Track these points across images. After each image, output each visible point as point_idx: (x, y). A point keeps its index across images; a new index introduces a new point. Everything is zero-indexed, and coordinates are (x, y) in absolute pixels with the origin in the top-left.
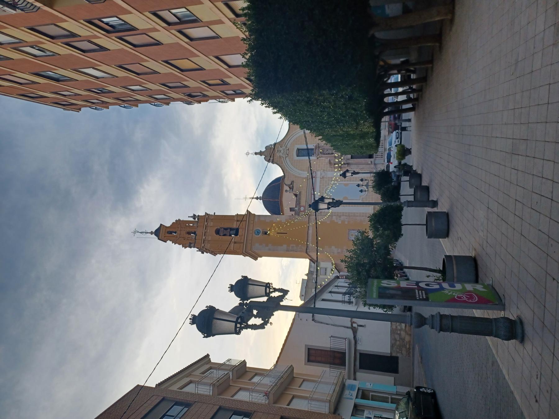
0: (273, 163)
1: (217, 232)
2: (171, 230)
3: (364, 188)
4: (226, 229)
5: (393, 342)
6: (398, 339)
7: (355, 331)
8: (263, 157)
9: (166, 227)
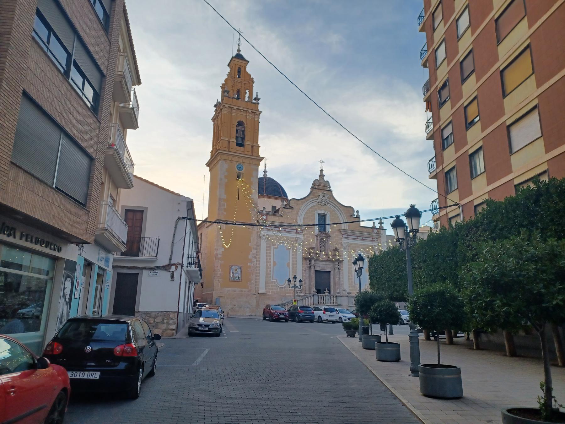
0: (312, 188)
1: (240, 123)
2: (242, 72)
3: (292, 284)
4: (243, 132)
5: (153, 314)
6: (156, 320)
7: (166, 268)
8: (318, 178)
9: (245, 67)
